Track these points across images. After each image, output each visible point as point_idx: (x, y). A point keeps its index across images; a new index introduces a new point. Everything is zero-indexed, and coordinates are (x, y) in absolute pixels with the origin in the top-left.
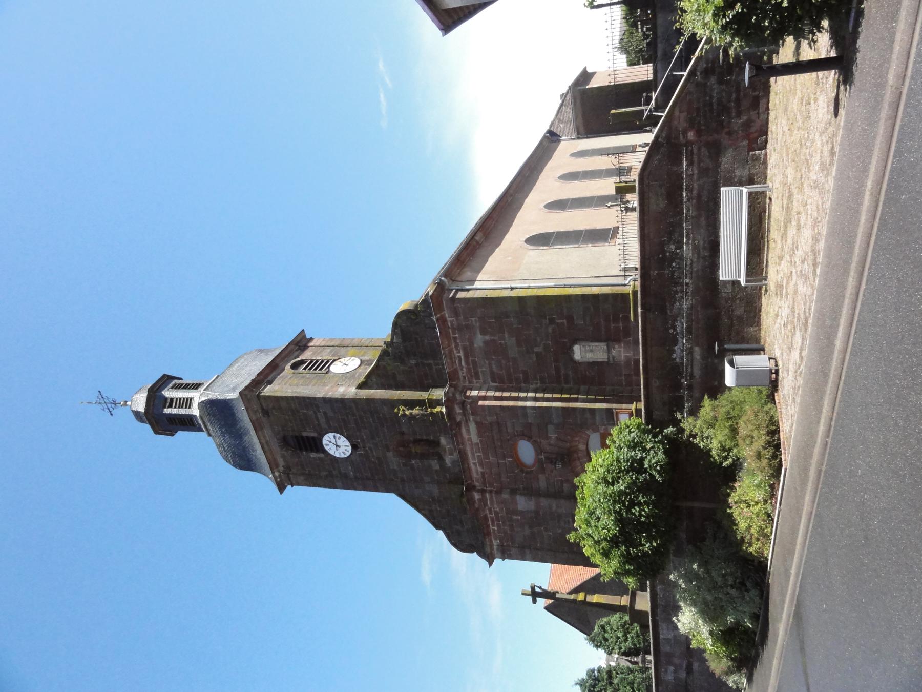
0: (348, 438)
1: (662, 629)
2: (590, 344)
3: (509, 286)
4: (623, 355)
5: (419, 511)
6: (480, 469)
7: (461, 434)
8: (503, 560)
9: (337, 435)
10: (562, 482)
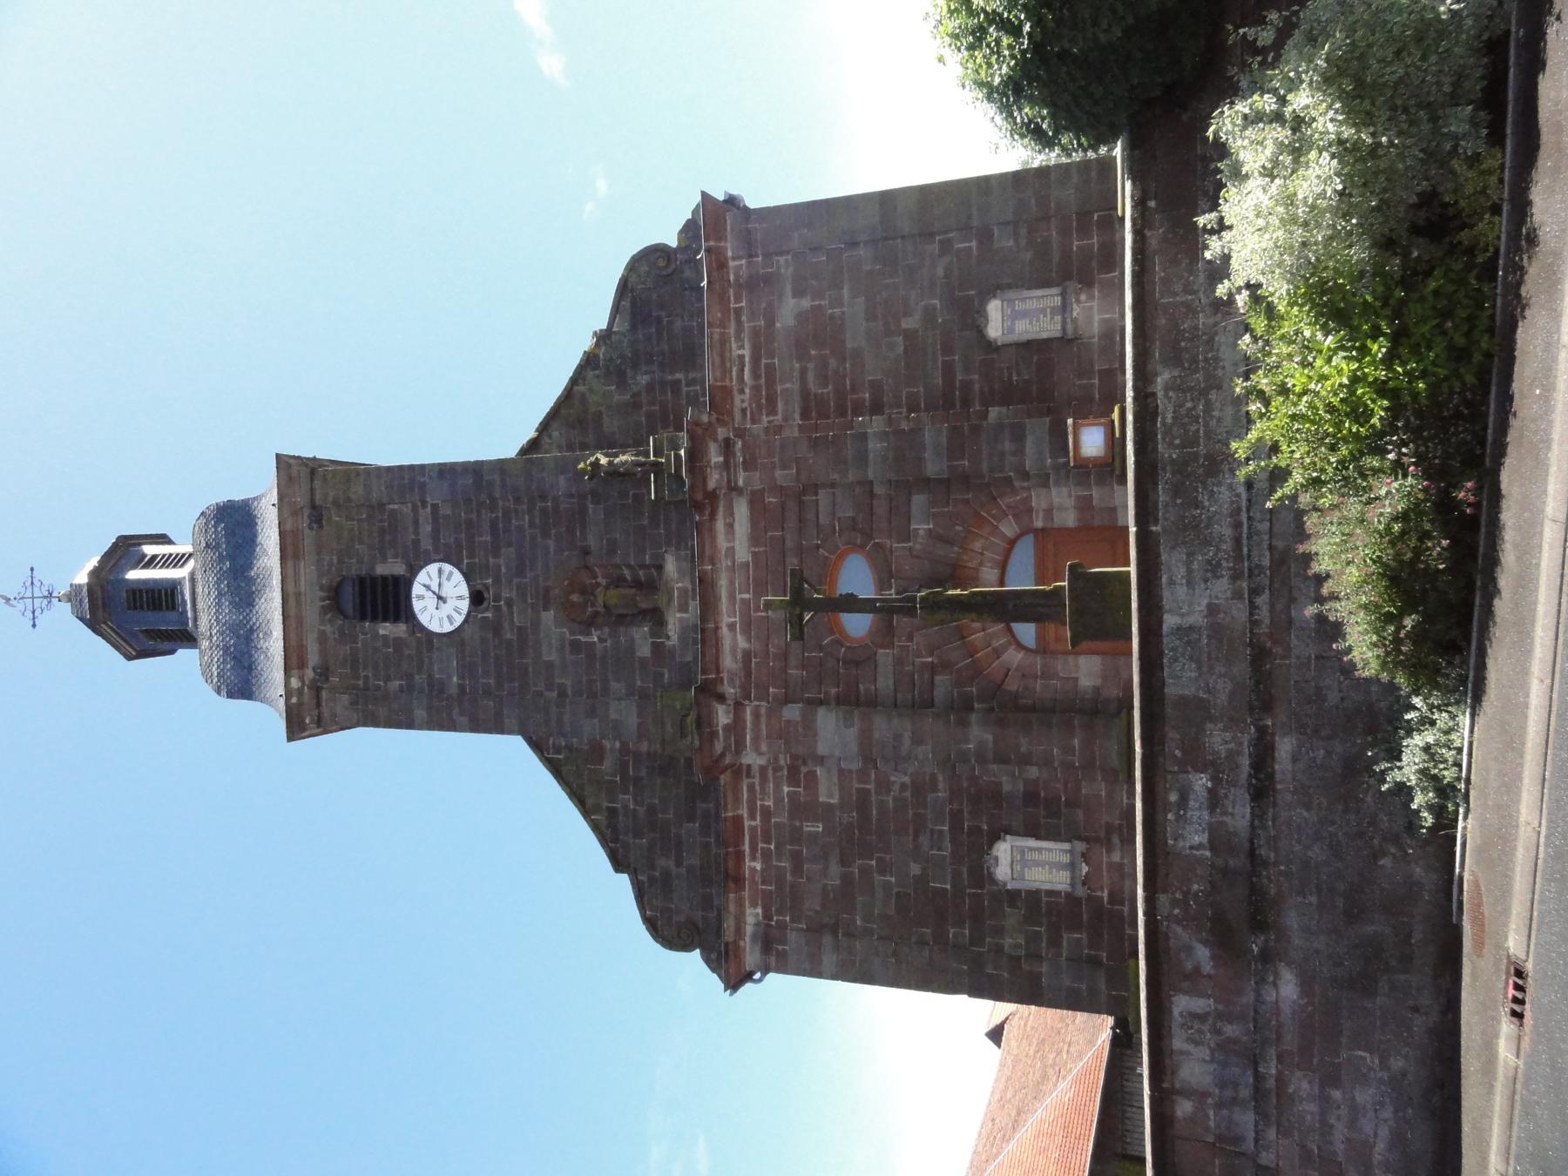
0: (467, 577)
1: (1172, 582)
2: (1026, 293)
4: (1096, 318)
5: (586, 813)
6: (742, 643)
7: (712, 530)
9: (447, 567)
10: (933, 669)
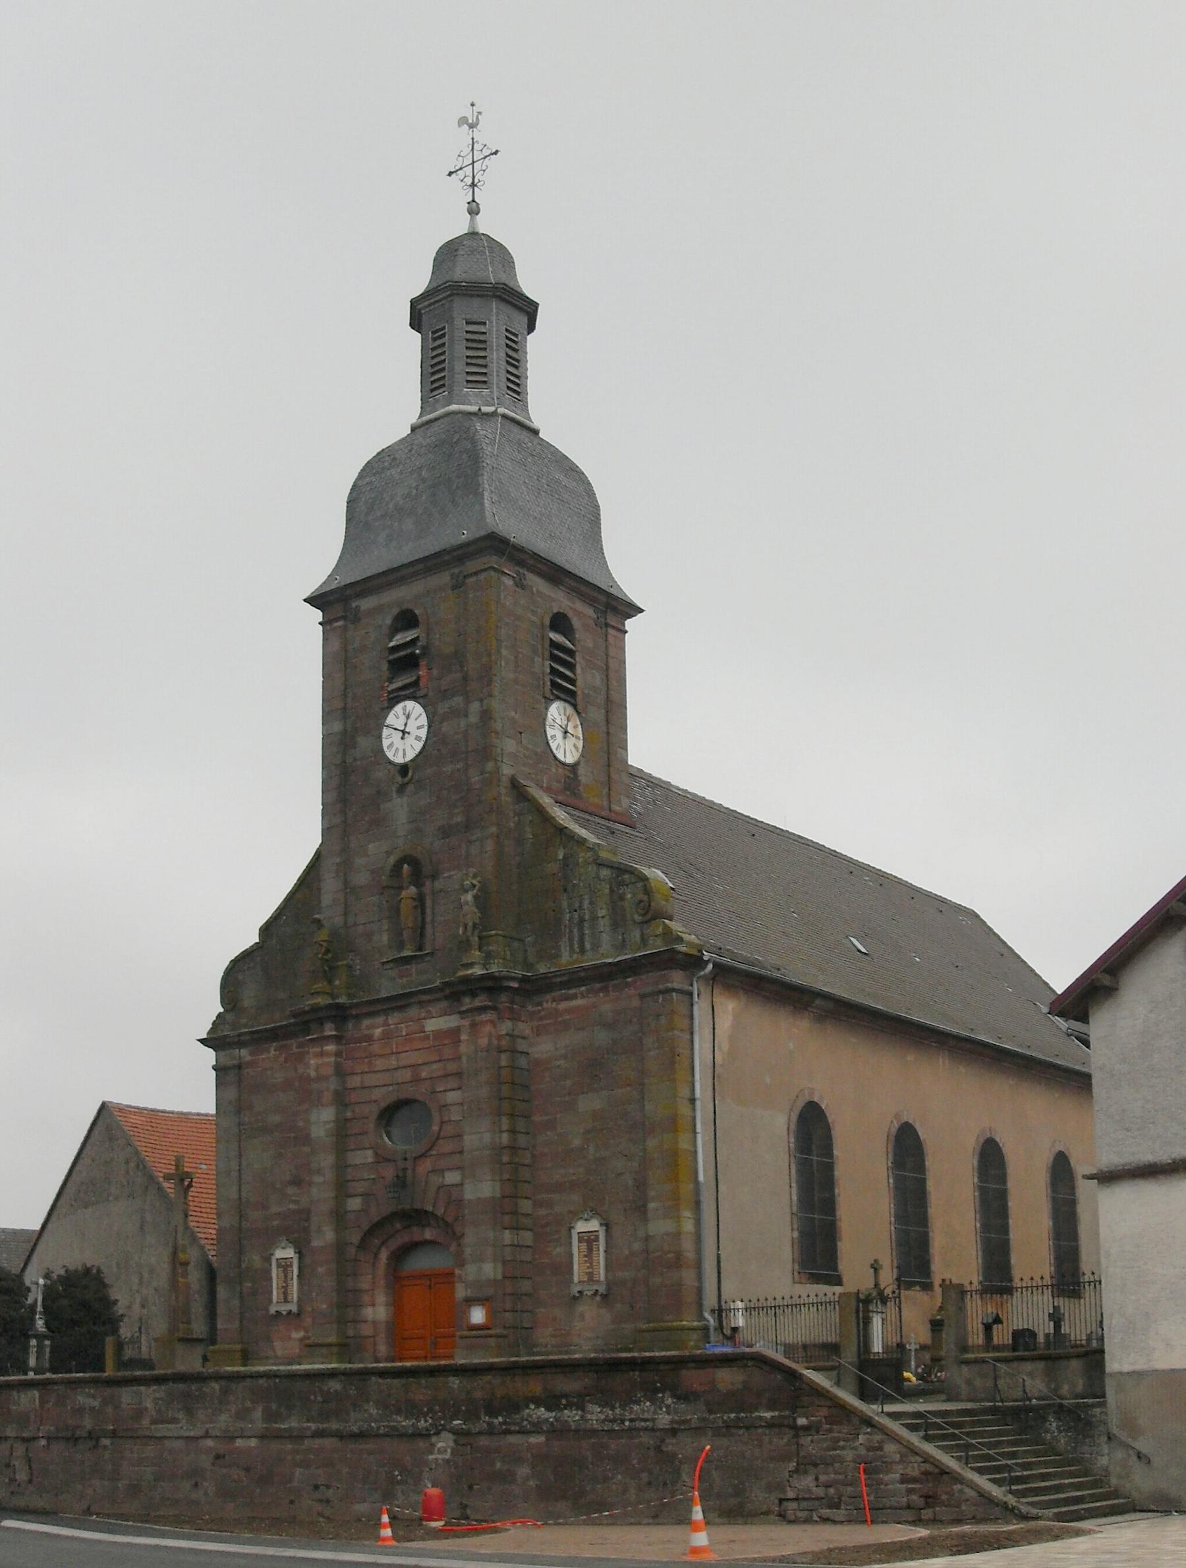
3: (698, 1093)
8: (214, 1068)
